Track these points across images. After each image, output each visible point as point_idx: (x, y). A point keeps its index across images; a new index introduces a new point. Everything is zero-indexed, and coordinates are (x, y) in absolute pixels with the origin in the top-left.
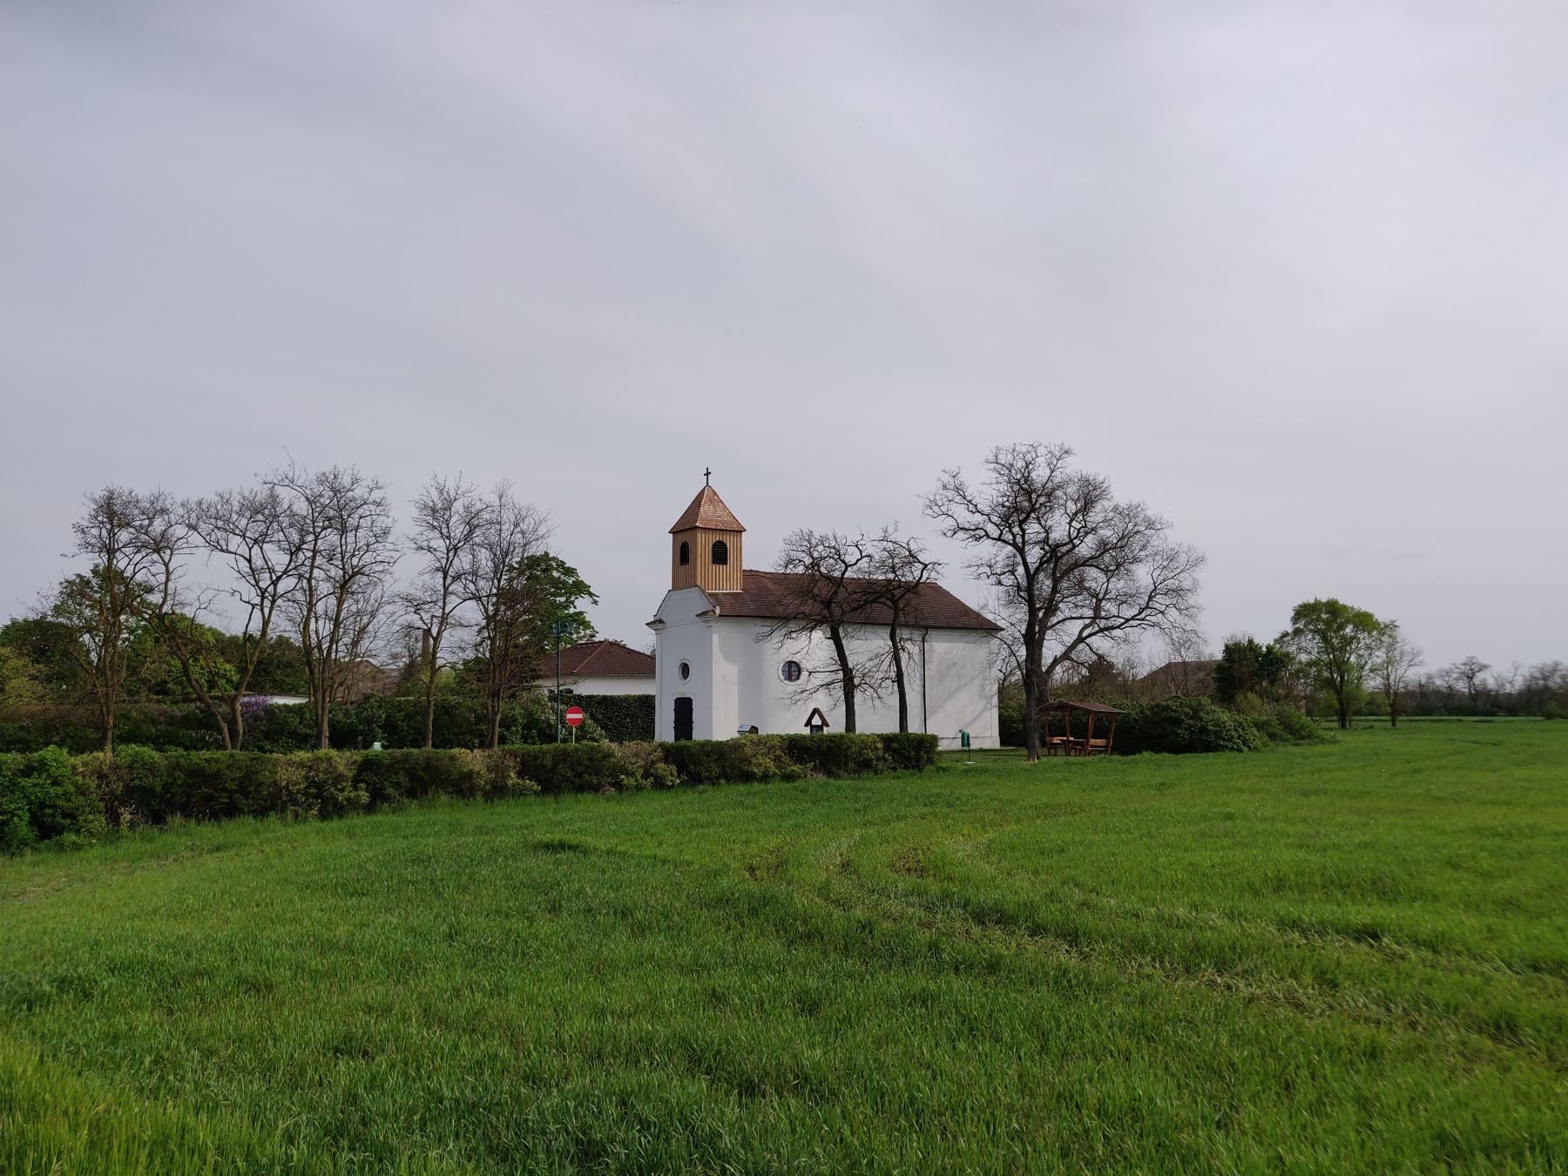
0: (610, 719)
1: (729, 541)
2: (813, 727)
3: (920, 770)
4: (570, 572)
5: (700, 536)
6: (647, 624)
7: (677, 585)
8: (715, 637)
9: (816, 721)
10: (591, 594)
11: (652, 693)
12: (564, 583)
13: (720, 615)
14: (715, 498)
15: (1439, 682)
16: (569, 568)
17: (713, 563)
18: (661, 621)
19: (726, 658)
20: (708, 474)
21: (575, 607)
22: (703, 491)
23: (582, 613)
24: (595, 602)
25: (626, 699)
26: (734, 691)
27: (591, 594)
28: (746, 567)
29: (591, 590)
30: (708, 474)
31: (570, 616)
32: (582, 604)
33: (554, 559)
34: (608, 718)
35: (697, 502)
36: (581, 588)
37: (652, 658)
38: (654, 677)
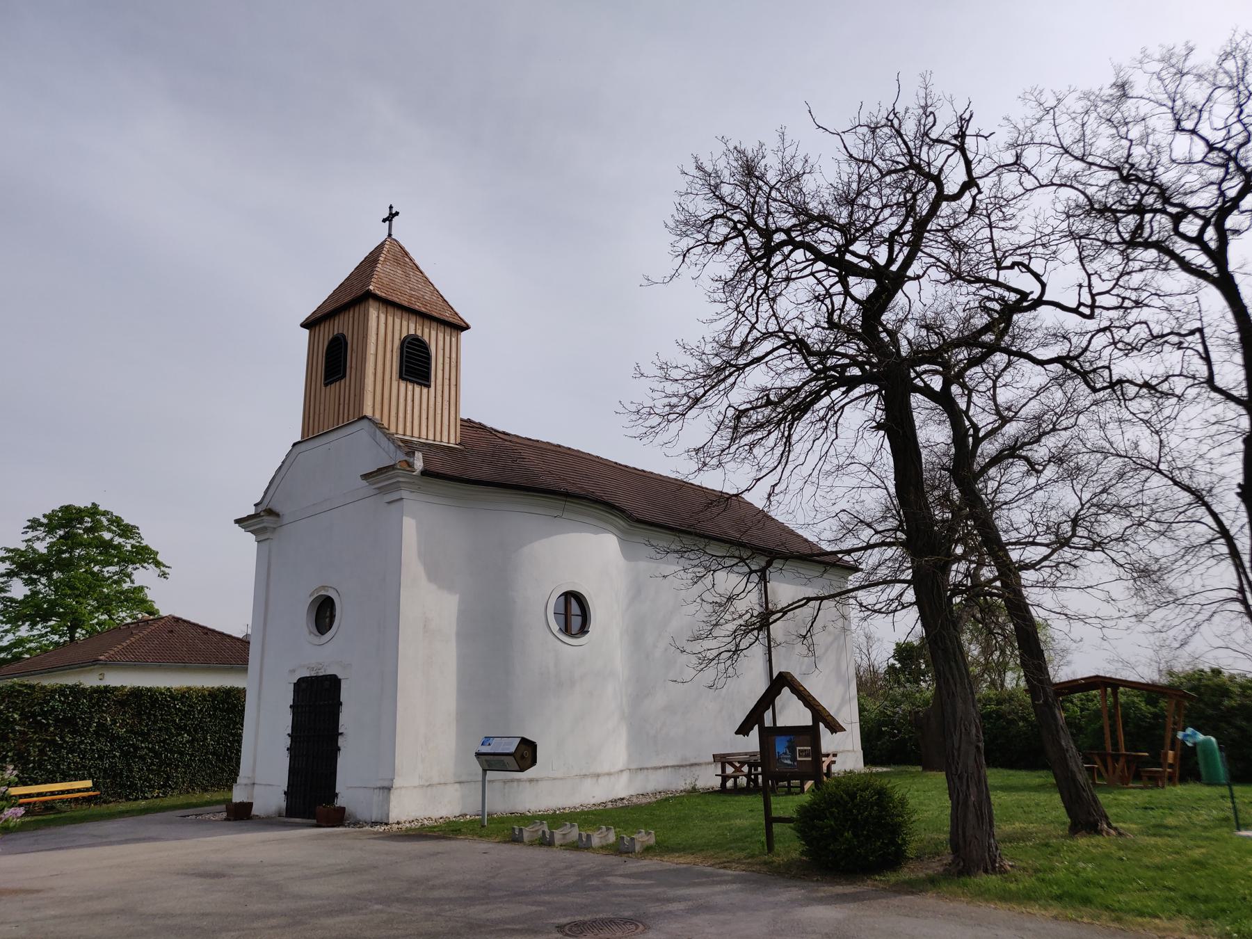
0: (145, 736)
1: (434, 338)
2: (768, 735)
3: (900, 825)
4: (127, 531)
5: (375, 317)
6: (238, 521)
7: (314, 427)
8: (409, 527)
9: (792, 713)
10: (158, 564)
11: (241, 686)
12: (119, 547)
13: (425, 473)
14: (402, 256)
15: (1188, 668)
16: (127, 525)
17: (401, 377)
18: (270, 512)
19: (435, 574)
20: (390, 218)
21: (132, 582)
22: (382, 245)
23: (141, 589)
24: (164, 575)
25: (184, 696)
26: (448, 655)
27: (158, 564)
28: (464, 415)
29: (159, 558)
30: (390, 218)
31: (122, 593)
32: (143, 576)
33: (105, 513)
34: (142, 734)
35: (371, 261)
36: (144, 555)
37: (244, 643)
38: (246, 670)
